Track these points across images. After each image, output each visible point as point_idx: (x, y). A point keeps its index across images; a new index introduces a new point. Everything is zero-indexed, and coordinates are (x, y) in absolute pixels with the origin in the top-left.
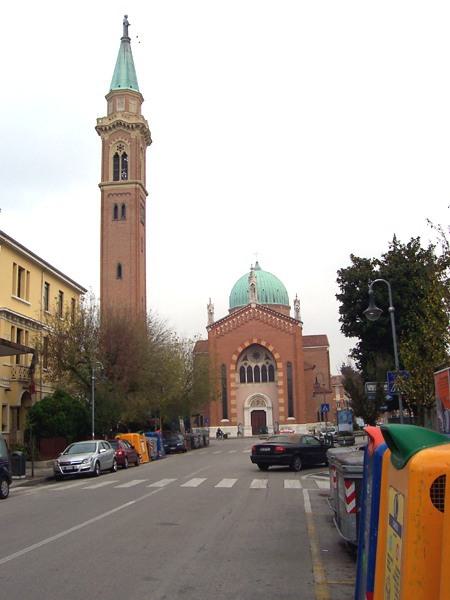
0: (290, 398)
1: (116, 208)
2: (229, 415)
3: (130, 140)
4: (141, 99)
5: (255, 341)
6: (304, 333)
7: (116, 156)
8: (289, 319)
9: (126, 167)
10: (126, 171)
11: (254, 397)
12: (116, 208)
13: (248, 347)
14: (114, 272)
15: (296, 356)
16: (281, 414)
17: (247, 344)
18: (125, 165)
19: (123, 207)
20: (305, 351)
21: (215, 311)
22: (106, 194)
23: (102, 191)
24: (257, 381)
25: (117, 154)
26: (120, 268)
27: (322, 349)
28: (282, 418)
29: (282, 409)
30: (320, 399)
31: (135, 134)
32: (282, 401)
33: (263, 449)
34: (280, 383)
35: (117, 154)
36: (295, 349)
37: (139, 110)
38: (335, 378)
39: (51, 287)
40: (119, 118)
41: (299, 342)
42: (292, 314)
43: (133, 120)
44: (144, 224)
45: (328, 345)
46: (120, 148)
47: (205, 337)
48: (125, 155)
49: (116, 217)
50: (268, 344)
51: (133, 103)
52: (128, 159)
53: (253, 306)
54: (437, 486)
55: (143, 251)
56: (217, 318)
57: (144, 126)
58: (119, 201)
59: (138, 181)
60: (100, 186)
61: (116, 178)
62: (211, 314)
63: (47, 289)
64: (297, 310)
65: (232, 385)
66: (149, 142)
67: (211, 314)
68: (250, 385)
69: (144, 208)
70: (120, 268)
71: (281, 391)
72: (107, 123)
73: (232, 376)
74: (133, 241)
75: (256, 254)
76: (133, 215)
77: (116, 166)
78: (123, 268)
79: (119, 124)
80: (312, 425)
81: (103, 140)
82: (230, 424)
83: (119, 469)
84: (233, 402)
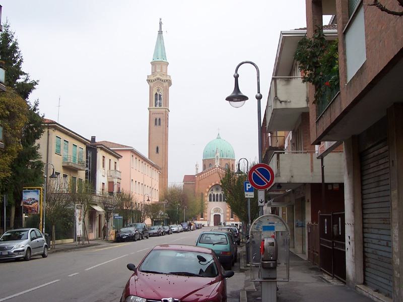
1: (156, 119)
7: (156, 94)
12: (156, 119)
17: (213, 184)
19: (160, 119)
23: (150, 112)
24: (217, 201)
26: (157, 148)
29: (228, 215)
40: (158, 76)
49: (156, 124)
51: (164, 67)
53: (217, 166)
58: (158, 117)
70: (157, 148)
77: (156, 99)
78: (159, 149)
82: (204, 220)
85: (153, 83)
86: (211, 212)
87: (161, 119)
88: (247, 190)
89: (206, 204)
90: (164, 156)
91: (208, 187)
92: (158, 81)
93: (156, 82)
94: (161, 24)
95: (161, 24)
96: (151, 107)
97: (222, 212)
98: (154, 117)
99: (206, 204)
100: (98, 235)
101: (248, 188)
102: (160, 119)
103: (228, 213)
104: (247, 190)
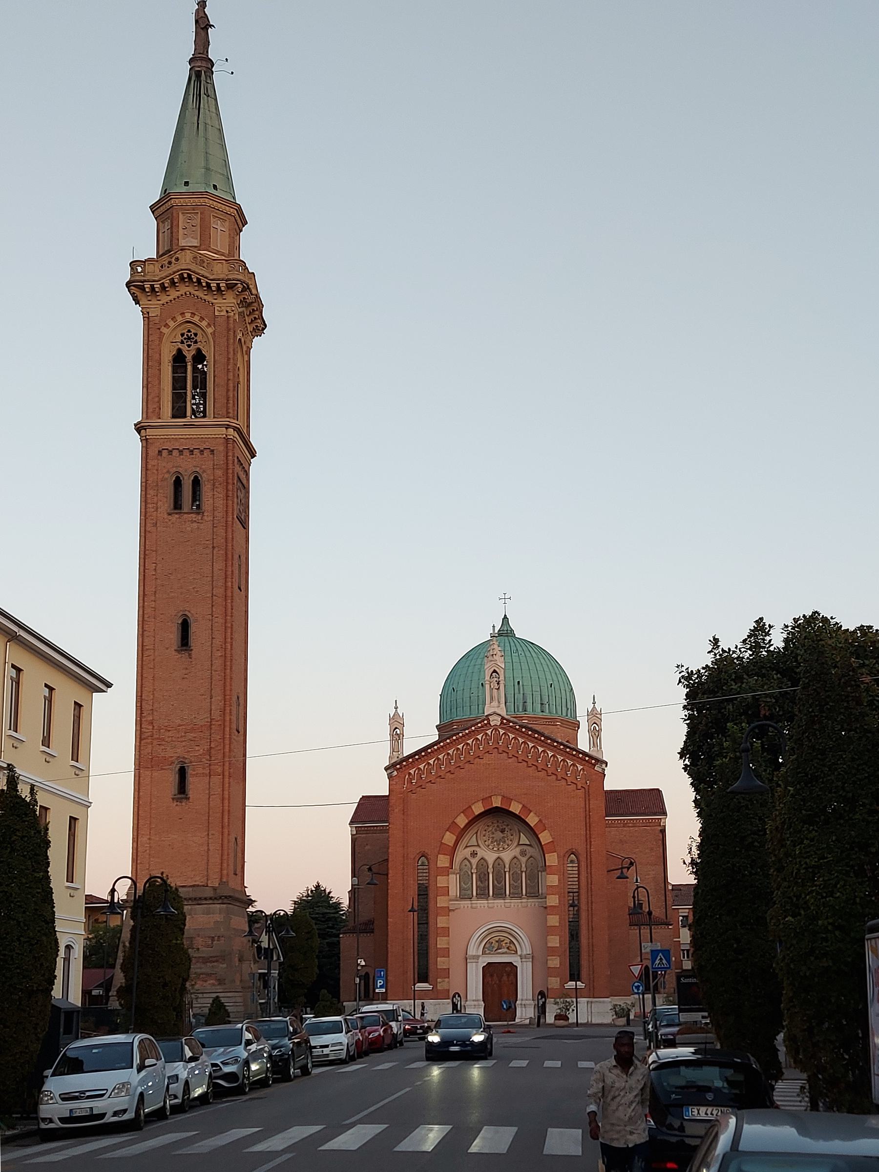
0: (574, 935)
1: (178, 483)
2: (431, 975)
3: (213, 322)
4: (239, 220)
5: (497, 802)
6: (609, 785)
7: (179, 359)
8: (571, 750)
9: (204, 386)
10: (204, 396)
11: (490, 932)
12: (178, 483)
13: (482, 815)
14: (173, 636)
15: (588, 840)
16: (550, 972)
17: (478, 809)
18: (200, 381)
19: (196, 482)
20: (609, 825)
21: (408, 731)
22: (153, 451)
23: (145, 441)
24: (499, 894)
25: (179, 351)
26: (185, 626)
27: (648, 823)
28: (554, 982)
29: (554, 962)
30: (778, 874)
31: (227, 303)
32: (554, 941)
33: (258, 1086)
34: (553, 900)
35: (179, 351)
36: (588, 826)
37: (234, 246)
38: (677, 888)
39: (24, 677)
40: (186, 261)
41: (598, 805)
42: (583, 743)
43: (220, 271)
44: (244, 524)
45: (665, 814)
46: (189, 339)
47: (381, 787)
48: (199, 357)
49: (177, 505)
50: (527, 809)
51: (219, 229)
52: (208, 367)
53: (495, 721)
54: (123, 1086)
55: (242, 731)
56: (410, 747)
57: (247, 288)
58: (187, 467)
59: (234, 422)
60: (139, 428)
61: (179, 412)
62: (397, 736)
63: (17, 682)
64: (595, 734)
65: (442, 902)
66: (260, 328)
67: (397, 736)
68: (483, 902)
69: (246, 488)
70: (185, 626)
71: (553, 920)
72: (156, 273)
73: (441, 881)
74: (219, 565)
75: (505, 599)
76: (220, 503)
77: (179, 384)
78: (193, 628)
79: (186, 278)
80: (620, 1001)
81: (147, 317)
82: (435, 994)
83: (275, 1081)
84: (441, 943)
85: (164, 299)
86: (472, 951)
87: (204, 478)
88: (378, 986)
89: (448, 911)
90: (218, 663)
91: (467, 810)
92: (183, 289)
93: (173, 294)
94: (203, 25)
95: (203, 25)
96: (155, 422)
97: (525, 947)
98: (167, 467)
99: (448, 911)
100: (145, 416)
101: (379, 984)
102: (196, 482)
103: (552, 951)
104: (378, 986)
